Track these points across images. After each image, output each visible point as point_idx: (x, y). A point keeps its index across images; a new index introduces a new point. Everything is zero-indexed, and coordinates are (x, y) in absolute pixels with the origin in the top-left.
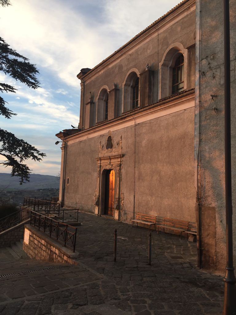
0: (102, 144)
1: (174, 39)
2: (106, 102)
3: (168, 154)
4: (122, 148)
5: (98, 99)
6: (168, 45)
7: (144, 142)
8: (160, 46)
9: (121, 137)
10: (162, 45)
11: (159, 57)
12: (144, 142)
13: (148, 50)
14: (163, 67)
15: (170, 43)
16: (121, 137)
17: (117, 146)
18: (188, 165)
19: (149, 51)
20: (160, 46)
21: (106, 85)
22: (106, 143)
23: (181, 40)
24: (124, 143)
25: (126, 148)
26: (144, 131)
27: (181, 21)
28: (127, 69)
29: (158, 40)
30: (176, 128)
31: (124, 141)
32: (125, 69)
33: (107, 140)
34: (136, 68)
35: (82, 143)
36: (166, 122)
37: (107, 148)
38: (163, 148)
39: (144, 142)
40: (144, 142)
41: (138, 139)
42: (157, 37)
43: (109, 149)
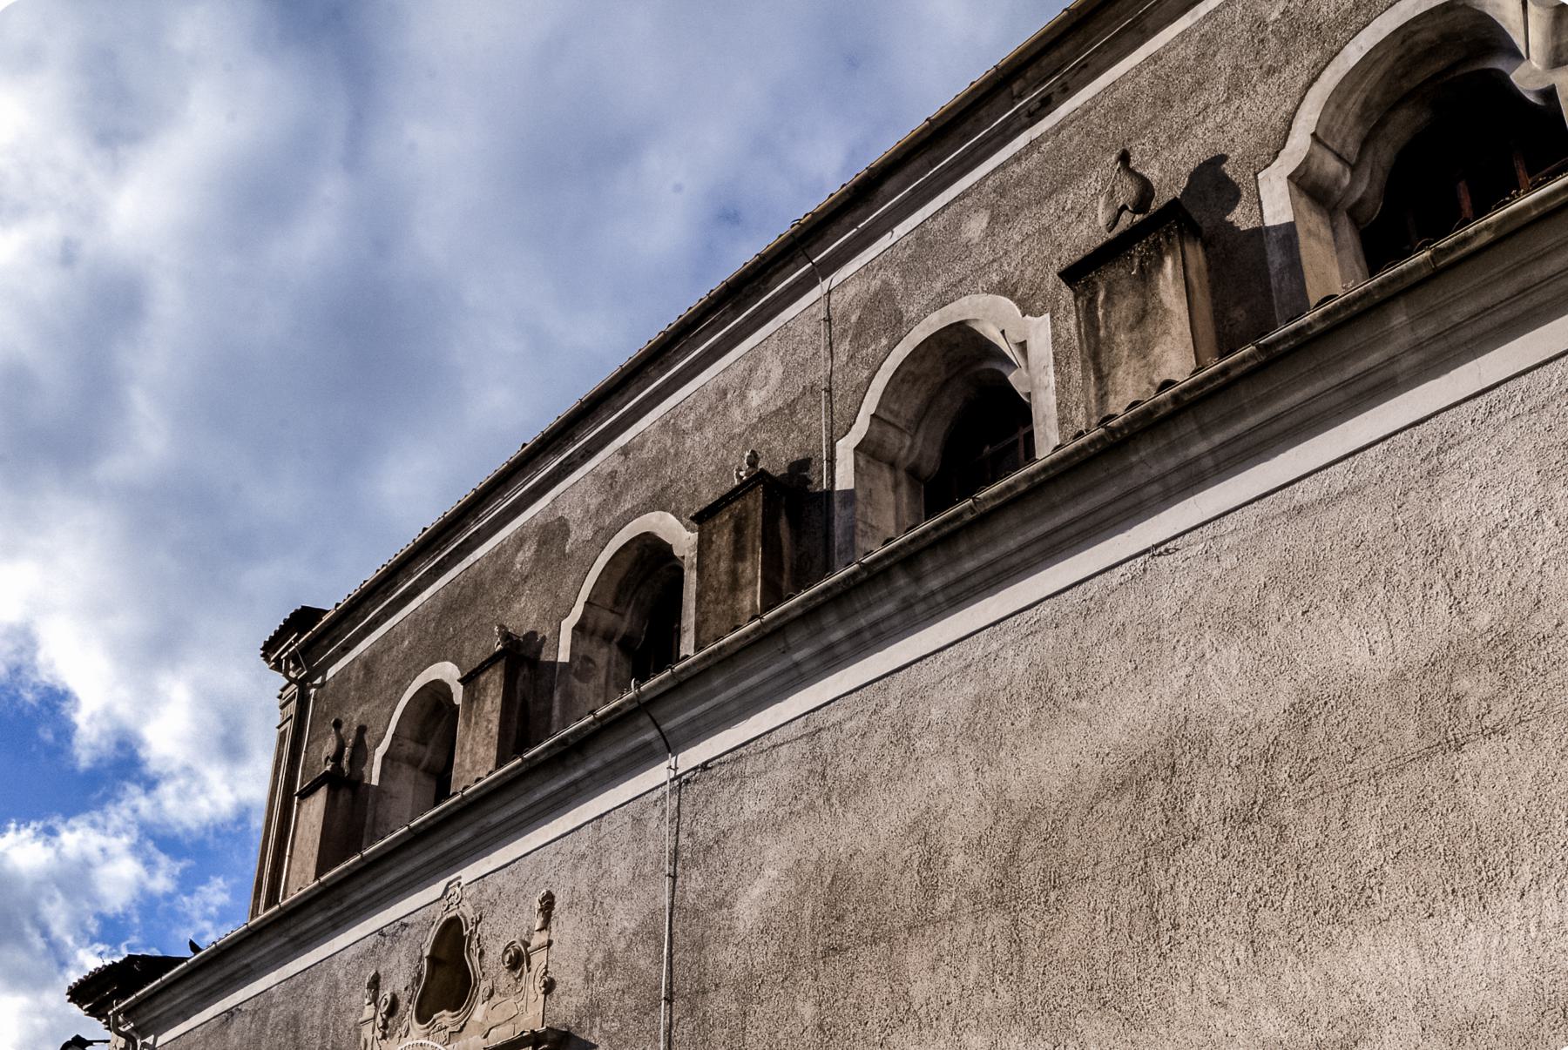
0: (386, 994)
1: (938, 286)
2: (433, 784)
3: (1001, 947)
4: (549, 987)
5: (385, 757)
6: (897, 326)
7: (757, 891)
8: (844, 347)
9: (548, 903)
10: (856, 337)
11: (837, 407)
12: (752, 903)
13: (752, 393)
14: (862, 463)
15: (913, 311)
16: (548, 903)
17: (505, 979)
18: (1236, 1003)
19: (755, 398)
20: (844, 347)
21: (445, 659)
22: (418, 979)
23: (995, 278)
24: (568, 948)
25: (588, 979)
26: (752, 807)
27: (989, 182)
28: (596, 533)
29: (828, 320)
30: (1074, 712)
31: (566, 926)
32: (580, 534)
33: (427, 952)
34: (664, 509)
35: (237, 1023)
36: (970, 689)
37: (423, 1017)
38: (944, 903)
39: (757, 891)
40: (752, 903)
41: (694, 882)
42: (822, 305)
43: (445, 1018)
